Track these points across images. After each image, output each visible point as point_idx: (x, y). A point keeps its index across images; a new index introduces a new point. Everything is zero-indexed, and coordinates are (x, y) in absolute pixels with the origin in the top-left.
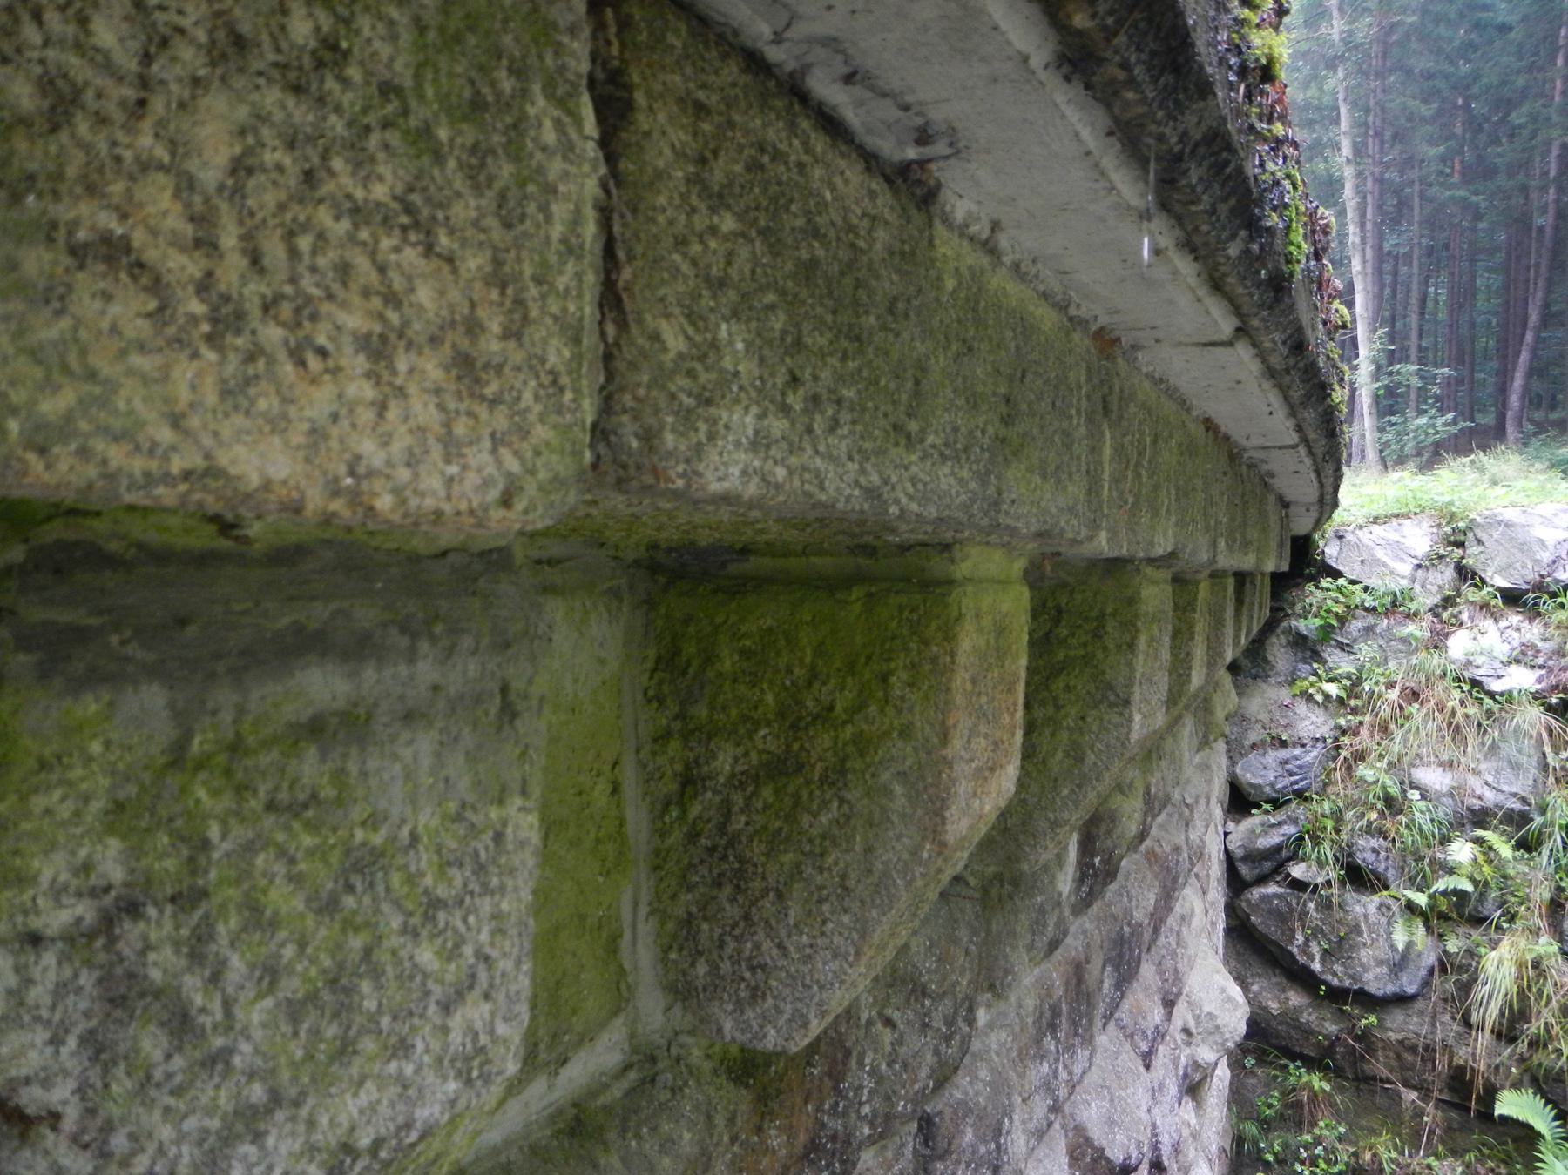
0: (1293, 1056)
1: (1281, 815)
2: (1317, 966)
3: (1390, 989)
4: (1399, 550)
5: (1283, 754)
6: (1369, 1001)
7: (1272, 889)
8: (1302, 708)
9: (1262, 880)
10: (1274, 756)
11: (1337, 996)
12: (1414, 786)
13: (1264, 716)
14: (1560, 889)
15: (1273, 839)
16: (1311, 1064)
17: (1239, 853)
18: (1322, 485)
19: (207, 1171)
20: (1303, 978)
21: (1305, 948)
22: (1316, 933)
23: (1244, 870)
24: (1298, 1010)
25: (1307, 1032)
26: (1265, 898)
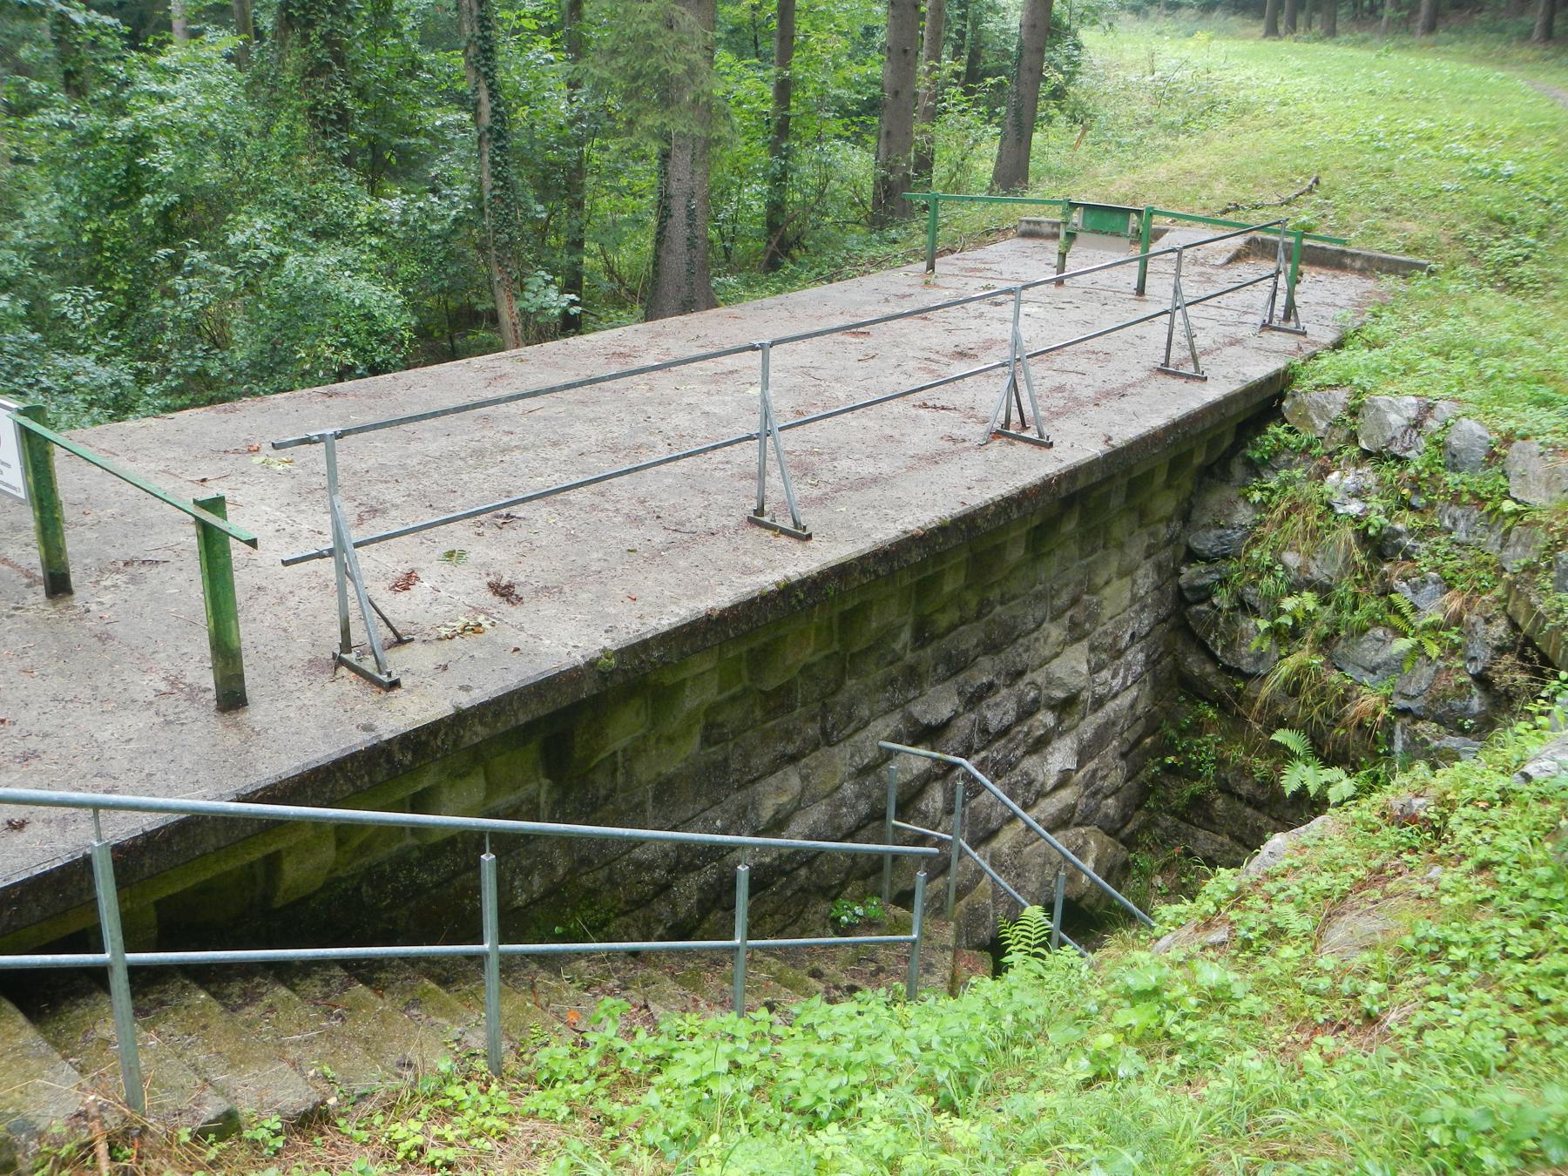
0: (1204, 699)
1: (1212, 568)
2: (1219, 653)
3: (1253, 670)
4: (1322, 411)
5: (1220, 532)
6: (1239, 673)
7: (1204, 607)
8: (1241, 506)
9: (1200, 601)
10: (1213, 533)
11: (1228, 670)
12: (1281, 562)
13: (1216, 508)
14: (1122, 7)
15: (1207, 580)
16: (1212, 704)
17: (1185, 586)
18: (1291, 294)
19: (5, 205)
20: (1213, 659)
21: (1214, 642)
22: (1222, 635)
23: (1188, 595)
24: (1209, 675)
25: (1210, 687)
26: (1198, 612)
